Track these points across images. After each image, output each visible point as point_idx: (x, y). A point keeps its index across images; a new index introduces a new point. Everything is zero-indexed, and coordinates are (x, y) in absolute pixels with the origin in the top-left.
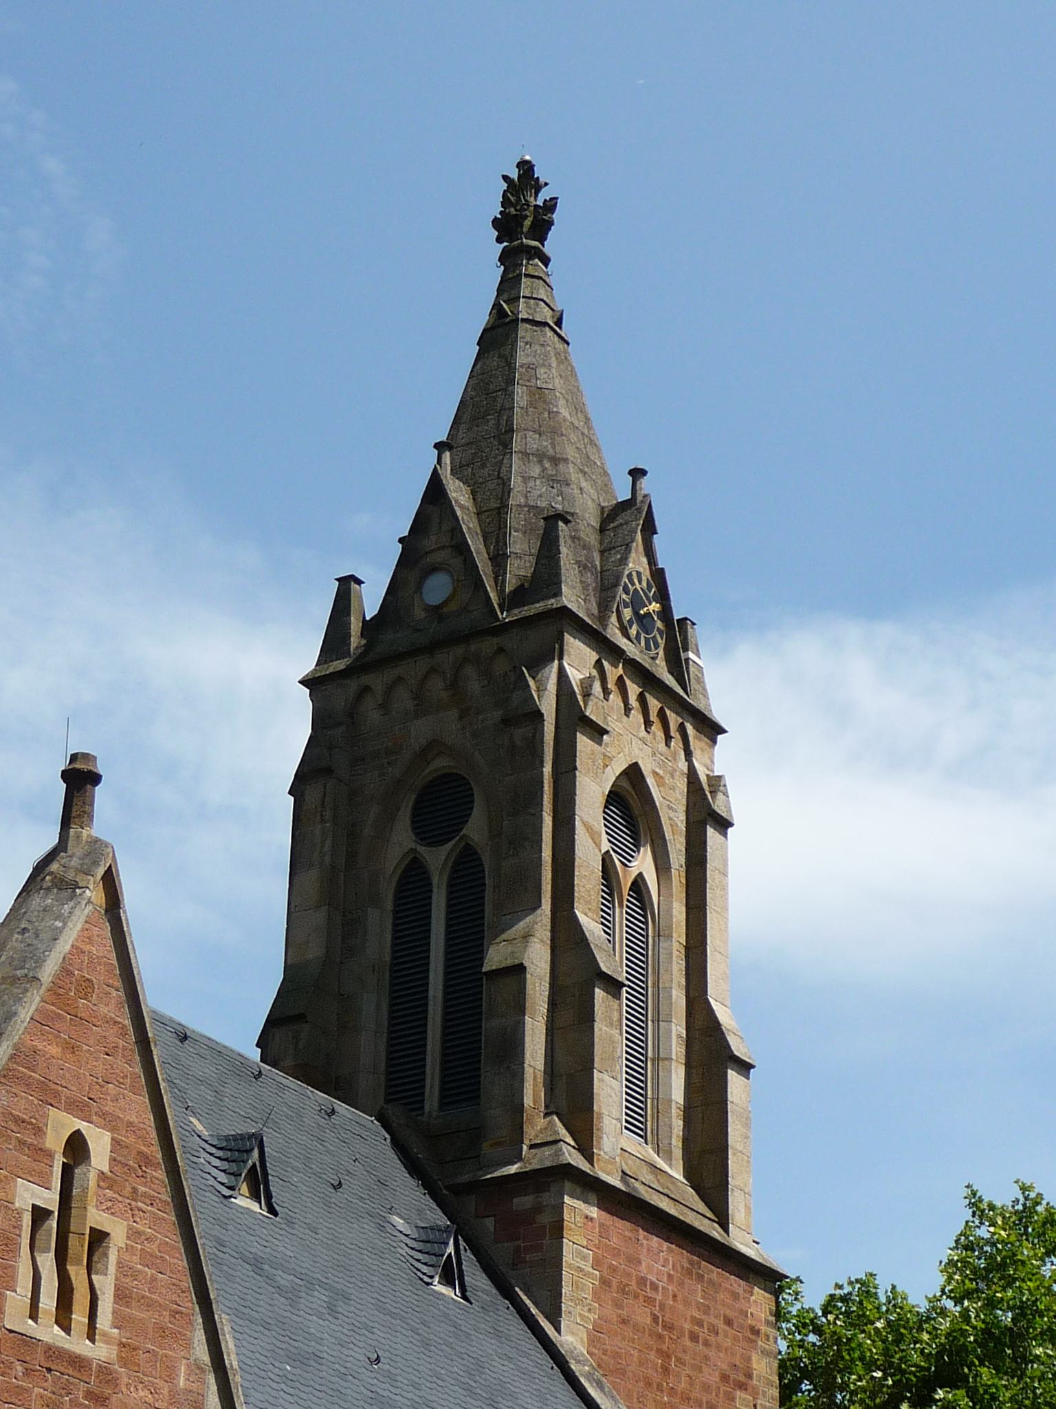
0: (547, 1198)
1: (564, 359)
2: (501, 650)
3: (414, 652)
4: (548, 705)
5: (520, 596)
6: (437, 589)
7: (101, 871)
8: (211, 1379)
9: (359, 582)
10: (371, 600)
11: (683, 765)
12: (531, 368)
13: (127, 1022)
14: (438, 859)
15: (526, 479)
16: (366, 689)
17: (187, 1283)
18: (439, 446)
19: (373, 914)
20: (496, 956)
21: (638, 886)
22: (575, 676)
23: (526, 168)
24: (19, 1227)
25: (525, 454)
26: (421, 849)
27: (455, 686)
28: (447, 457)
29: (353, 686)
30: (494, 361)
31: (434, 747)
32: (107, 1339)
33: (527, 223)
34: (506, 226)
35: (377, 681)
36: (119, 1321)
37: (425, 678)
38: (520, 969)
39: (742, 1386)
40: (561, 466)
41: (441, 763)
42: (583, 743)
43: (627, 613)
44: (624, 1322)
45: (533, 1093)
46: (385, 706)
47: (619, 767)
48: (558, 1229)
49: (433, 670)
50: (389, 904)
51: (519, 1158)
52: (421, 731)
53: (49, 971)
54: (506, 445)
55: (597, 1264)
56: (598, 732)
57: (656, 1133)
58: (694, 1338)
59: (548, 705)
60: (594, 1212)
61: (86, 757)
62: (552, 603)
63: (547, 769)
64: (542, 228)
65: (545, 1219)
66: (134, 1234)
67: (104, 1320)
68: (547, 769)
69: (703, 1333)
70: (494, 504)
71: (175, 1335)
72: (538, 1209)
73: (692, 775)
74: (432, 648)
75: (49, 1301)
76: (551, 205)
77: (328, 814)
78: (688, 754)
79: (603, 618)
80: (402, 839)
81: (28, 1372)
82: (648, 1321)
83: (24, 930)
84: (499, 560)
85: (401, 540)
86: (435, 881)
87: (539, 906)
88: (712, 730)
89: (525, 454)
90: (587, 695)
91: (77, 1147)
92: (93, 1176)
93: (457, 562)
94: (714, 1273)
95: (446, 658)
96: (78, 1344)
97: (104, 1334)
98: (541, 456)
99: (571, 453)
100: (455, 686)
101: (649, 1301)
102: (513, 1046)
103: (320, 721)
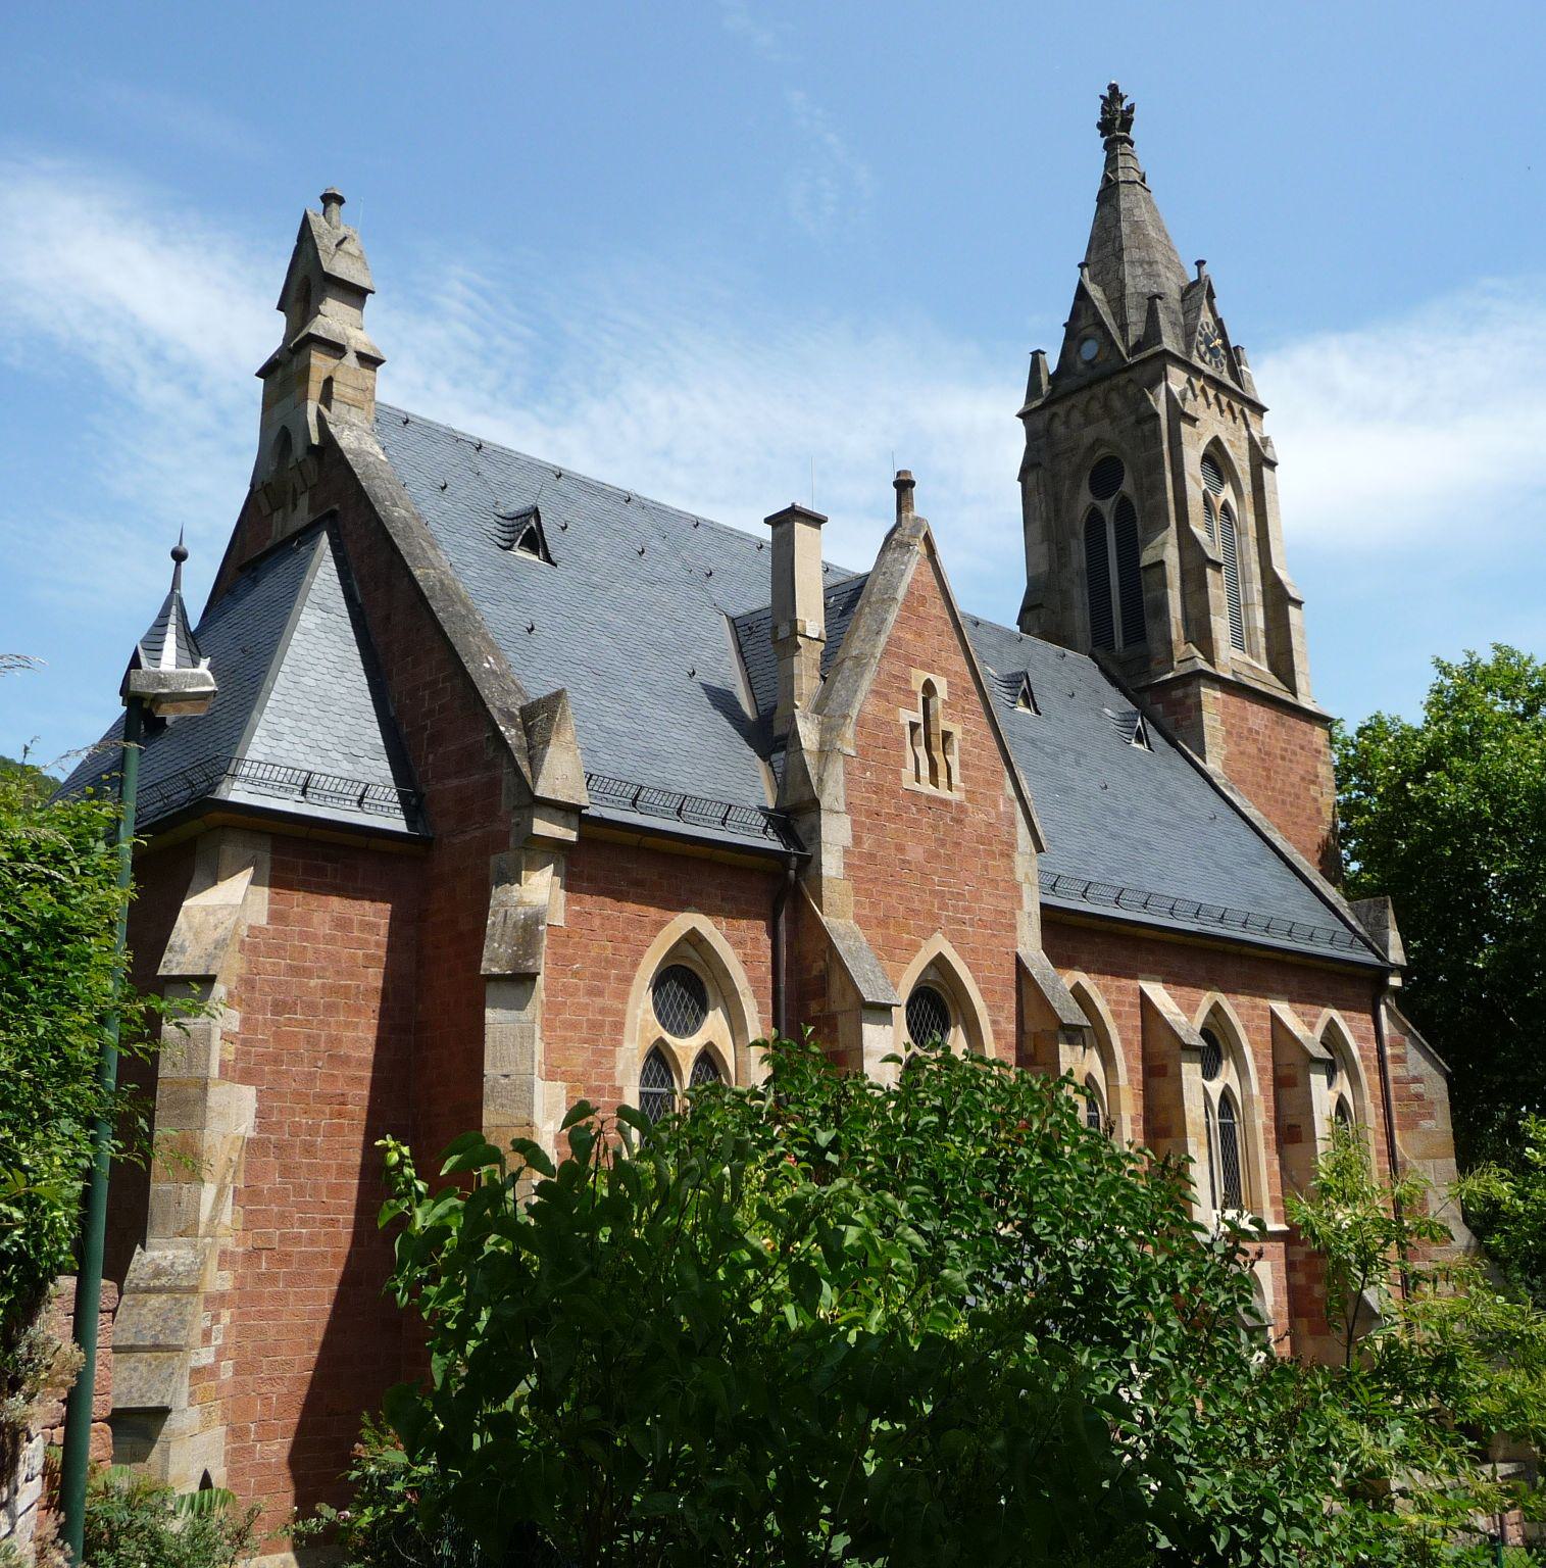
0: (1191, 690)
1: (1148, 202)
2: (1130, 380)
3: (1080, 389)
4: (1162, 409)
5: (1138, 347)
6: (1089, 350)
7: (922, 535)
8: (1017, 805)
9: (1043, 353)
10: (1052, 362)
11: (1245, 433)
12: (1130, 210)
13: (947, 617)
14: (1107, 507)
15: (1134, 277)
16: (1054, 415)
17: (998, 755)
18: (1081, 266)
19: (1074, 543)
20: (1147, 557)
21: (1225, 507)
22: (1176, 389)
23: (1113, 88)
24: (904, 734)
25: (1132, 262)
26: (1097, 502)
27: (1107, 407)
28: (1086, 270)
29: (1047, 414)
30: (1107, 210)
31: (1098, 442)
32: (959, 789)
33: (1118, 122)
34: (1105, 127)
35: (1060, 409)
36: (964, 779)
37: (1088, 402)
38: (1162, 563)
39: (1313, 782)
40: (1154, 266)
41: (1102, 452)
42: (1185, 427)
43: (1203, 348)
44: (1242, 753)
45: (1176, 632)
46: (1066, 423)
47: (1207, 439)
48: (1199, 707)
49: (1092, 398)
50: (1082, 536)
51: (1173, 669)
52: (1089, 434)
53: (901, 594)
54: (1120, 259)
55: (1223, 723)
56: (1193, 420)
57: (1250, 647)
58: (1283, 758)
59: (1162, 409)
60: (1219, 694)
61: (906, 472)
62: (1158, 348)
63: (1165, 446)
64: (1127, 124)
65: (1190, 701)
66: (966, 732)
67: (956, 779)
68: (1165, 446)
69: (1288, 755)
70: (1117, 295)
71: (995, 783)
72: (1186, 696)
73: (1251, 438)
74: (1089, 385)
75: (925, 772)
76: (1131, 109)
77: (1042, 489)
78: (1247, 426)
79: (1188, 353)
80: (1086, 498)
81: (919, 811)
82: (1256, 751)
83: (884, 573)
84: (1123, 328)
85: (1065, 325)
86: (1107, 519)
87: (1168, 525)
88: (1259, 410)
89: (1132, 262)
90: (1184, 399)
91: (929, 688)
92: (939, 703)
93: (1099, 333)
94: (1291, 721)
95: (1099, 390)
96: (943, 793)
97: (957, 786)
98: (1141, 262)
99: (1158, 257)
100: (1107, 407)
101: (1255, 741)
102: (1162, 608)
103: (1031, 437)
